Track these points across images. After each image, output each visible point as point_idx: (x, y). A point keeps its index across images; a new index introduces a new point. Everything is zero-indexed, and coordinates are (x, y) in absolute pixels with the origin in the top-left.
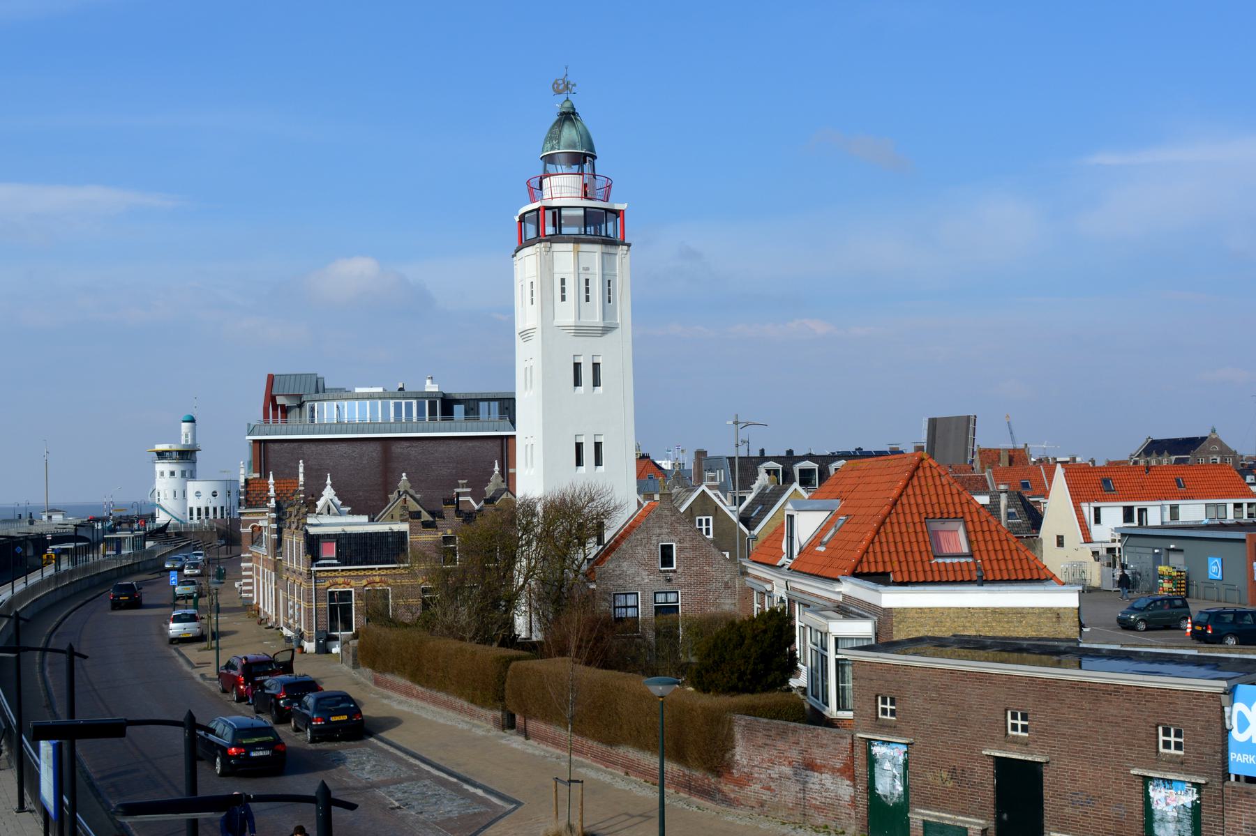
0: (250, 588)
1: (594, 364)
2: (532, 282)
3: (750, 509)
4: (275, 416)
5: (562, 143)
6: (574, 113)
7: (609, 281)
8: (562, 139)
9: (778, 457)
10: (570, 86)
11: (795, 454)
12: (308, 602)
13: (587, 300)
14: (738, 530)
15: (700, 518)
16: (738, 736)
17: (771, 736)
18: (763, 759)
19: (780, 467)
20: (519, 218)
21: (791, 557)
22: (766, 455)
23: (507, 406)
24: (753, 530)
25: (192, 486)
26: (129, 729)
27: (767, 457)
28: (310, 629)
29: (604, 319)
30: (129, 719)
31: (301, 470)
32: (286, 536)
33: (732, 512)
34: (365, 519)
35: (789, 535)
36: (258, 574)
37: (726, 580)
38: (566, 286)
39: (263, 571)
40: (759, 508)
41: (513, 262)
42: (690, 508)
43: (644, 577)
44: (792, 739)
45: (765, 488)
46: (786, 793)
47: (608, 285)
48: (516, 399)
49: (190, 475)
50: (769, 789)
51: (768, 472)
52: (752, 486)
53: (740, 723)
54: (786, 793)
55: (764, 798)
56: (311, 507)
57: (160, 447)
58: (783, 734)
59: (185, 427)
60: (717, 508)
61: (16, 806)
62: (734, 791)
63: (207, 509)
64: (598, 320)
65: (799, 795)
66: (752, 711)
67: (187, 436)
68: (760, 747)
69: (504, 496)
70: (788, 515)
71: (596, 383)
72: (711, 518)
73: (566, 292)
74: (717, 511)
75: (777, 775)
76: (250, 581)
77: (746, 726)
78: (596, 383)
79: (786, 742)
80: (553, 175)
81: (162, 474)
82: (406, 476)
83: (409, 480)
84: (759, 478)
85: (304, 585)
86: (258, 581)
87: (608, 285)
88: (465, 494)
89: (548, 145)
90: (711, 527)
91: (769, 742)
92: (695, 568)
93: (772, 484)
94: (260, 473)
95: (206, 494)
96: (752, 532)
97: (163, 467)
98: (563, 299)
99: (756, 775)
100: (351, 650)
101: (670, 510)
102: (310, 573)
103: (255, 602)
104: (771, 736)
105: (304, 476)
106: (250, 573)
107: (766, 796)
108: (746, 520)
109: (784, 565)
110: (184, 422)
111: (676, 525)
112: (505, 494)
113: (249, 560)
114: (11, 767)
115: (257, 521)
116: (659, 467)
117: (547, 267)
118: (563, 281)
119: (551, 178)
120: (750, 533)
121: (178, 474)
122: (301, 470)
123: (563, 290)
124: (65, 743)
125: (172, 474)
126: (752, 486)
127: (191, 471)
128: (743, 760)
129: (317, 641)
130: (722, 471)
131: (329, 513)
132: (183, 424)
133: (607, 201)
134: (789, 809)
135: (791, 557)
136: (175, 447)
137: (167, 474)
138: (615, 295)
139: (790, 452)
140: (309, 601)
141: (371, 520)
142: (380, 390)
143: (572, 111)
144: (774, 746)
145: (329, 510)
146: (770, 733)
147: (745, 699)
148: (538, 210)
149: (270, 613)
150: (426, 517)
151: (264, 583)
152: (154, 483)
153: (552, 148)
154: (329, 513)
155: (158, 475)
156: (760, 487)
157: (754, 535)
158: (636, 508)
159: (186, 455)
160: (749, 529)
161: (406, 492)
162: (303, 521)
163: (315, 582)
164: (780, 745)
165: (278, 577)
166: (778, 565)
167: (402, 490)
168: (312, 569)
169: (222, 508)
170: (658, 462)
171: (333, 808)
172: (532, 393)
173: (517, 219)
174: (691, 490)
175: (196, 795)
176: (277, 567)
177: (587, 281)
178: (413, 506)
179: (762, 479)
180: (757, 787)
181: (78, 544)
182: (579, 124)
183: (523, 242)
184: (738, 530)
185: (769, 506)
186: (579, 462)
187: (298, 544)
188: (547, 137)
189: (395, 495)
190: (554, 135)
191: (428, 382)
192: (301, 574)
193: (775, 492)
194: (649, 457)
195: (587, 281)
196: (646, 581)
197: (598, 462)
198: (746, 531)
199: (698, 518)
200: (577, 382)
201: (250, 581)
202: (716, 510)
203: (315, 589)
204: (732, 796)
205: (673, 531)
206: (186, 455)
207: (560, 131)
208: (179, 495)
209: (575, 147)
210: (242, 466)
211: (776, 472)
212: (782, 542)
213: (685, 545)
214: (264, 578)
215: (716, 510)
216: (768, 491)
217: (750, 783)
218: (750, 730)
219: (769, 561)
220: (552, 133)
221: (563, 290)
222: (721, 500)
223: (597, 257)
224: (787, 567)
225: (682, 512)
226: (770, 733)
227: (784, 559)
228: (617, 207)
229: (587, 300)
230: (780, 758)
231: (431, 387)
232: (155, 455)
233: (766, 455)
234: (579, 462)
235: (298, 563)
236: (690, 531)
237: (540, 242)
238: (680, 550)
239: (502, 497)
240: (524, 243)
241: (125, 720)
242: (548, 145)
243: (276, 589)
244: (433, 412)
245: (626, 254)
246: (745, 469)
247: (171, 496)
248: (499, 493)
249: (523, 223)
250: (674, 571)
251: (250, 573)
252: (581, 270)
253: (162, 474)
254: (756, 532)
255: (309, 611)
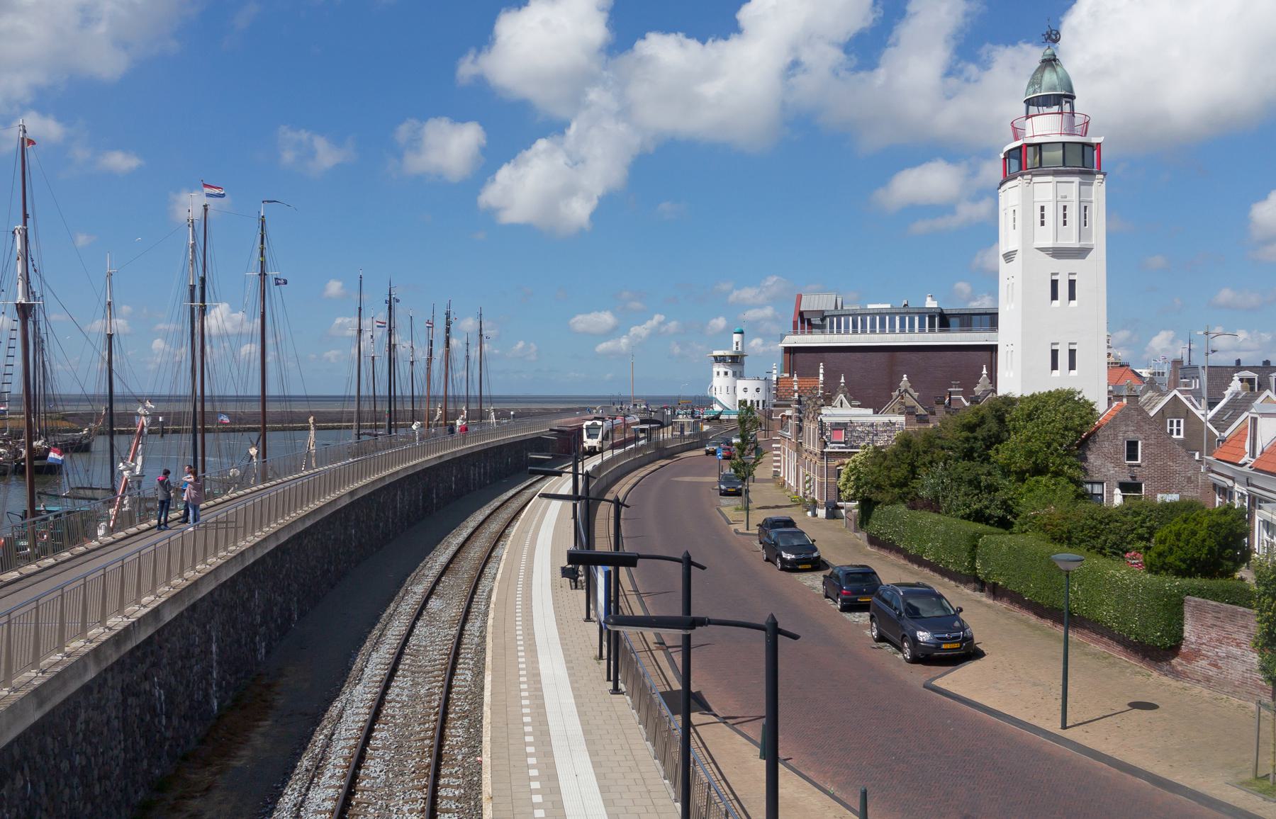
0: (779, 464)
1: (1070, 281)
2: (1014, 211)
3: (1222, 413)
4: (803, 328)
5: (1043, 87)
6: (1055, 60)
7: (1085, 207)
8: (1044, 83)
9: (1254, 367)
10: (1046, 36)
11: (1272, 365)
12: (821, 477)
13: (1065, 223)
14: (1205, 429)
15: (1178, 437)
16: (1187, 615)
17: (1220, 618)
18: (1211, 639)
19: (1256, 376)
20: (1004, 154)
21: (1254, 456)
22: (1242, 365)
23: (991, 320)
24: (1224, 432)
25: (741, 384)
26: (640, 562)
27: (1243, 367)
28: (822, 499)
29: (1080, 241)
30: (640, 554)
31: (821, 371)
32: (806, 423)
33: (1203, 413)
34: (870, 411)
35: (1252, 436)
36: (784, 453)
37: (1189, 475)
38: (1045, 213)
39: (788, 450)
40: (1231, 412)
41: (998, 194)
42: (1162, 410)
43: (1110, 469)
44: (1241, 623)
45: (1237, 394)
46: (1233, 672)
47: (1084, 210)
48: (999, 315)
49: (739, 375)
50: (1216, 666)
51: (1241, 380)
52: (1225, 392)
53: (1192, 600)
54: (1233, 672)
55: (1211, 673)
56: (828, 401)
57: (717, 353)
58: (1232, 617)
59: (736, 337)
60: (1188, 410)
61: (585, 617)
62: (1181, 664)
63: (758, 402)
64: (1074, 242)
65: (1246, 674)
66: (1201, 593)
67: (737, 344)
68: (1209, 627)
69: (990, 396)
70: (1252, 418)
71: (1072, 296)
72: (1182, 421)
73: (1045, 217)
74: (1188, 414)
75: (1224, 655)
76: (779, 458)
77: (1195, 607)
78: (1072, 296)
79: (1234, 625)
80: (1034, 116)
81: (718, 373)
82: (907, 377)
83: (909, 380)
84: (1232, 384)
85: (819, 463)
86: (784, 458)
87: (1084, 210)
88: (957, 393)
89: (1031, 90)
90: (1169, 428)
91: (1219, 623)
92: (1159, 463)
93: (1244, 391)
94: (790, 373)
95: (752, 390)
96: (1222, 434)
97: (719, 368)
98: (1043, 224)
99: (1204, 652)
100: (853, 518)
101: (1136, 410)
102: (823, 453)
103: (782, 475)
104: (1220, 618)
105: (824, 376)
106: (778, 452)
107: (1212, 672)
108: (1218, 422)
109: (1246, 464)
110: (735, 333)
111: (1142, 424)
112: (991, 394)
113: (778, 442)
114: (583, 589)
115: (784, 411)
116: (1138, 375)
117: (1028, 198)
118: (1042, 208)
119: (1033, 118)
120: (1220, 435)
121: (730, 372)
122: (821, 371)
123: (1042, 216)
124: (611, 568)
125: (726, 373)
126: (1225, 392)
127: (740, 372)
128: (1191, 637)
129: (827, 509)
130: (1198, 381)
131: (841, 406)
132: (735, 335)
133: (1085, 136)
134: (1235, 686)
135: (1254, 456)
136: (728, 353)
137: (722, 374)
138: (1091, 220)
139: (1267, 363)
140: (822, 476)
141: (876, 412)
142: (888, 306)
143: (1053, 57)
144: (1223, 628)
145: (841, 403)
146: (1219, 615)
147: (1198, 582)
148: (1020, 148)
149: (792, 484)
150: (921, 411)
151: (788, 460)
152: (712, 380)
153: (1034, 93)
154: (841, 406)
155: (715, 374)
156: (1232, 394)
157: (1224, 437)
158: (1107, 407)
159: (736, 361)
160: (1220, 432)
161: (906, 391)
162: (819, 411)
163: (827, 461)
164: (1229, 627)
165: (799, 456)
166: (1240, 463)
167: (902, 389)
168: (825, 450)
169: (764, 401)
170: (1138, 371)
171: (779, 636)
172: (1012, 306)
173: (1002, 156)
174: (1163, 395)
175: (690, 615)
176: (799, 447)
177: (1065, 207)
178: (909, 401)
179: (1236, 385)
180: (1204, 663)
181: (652, 426)
182: (1059, 69)
183: (1008, 175)
184: (1205, 429)
185: (1240, 411)
186: (1054, 366)
187: (814, 429)
188: (1029, 83)
189: (897, 393)
190: (1035, 81)
191: (929, 299)
192: (816, 455)
193: (1247, 398)
194: (1128, 366)
195: (1065, 207)
196: (1112, 472)
197: (1072, 366)
198: (1217, 433)
199: (1168, 421)
200: (1054, 296)
201: (779, 458)
202: (1187, 413)
203: (827, 466)
204: (1179, 668)
205: (1139, 428)
206: (736, 361)
207: (1042, 77)
208: (731, 390)
209: (1055, 89)
210: (775, 367)
211: (1250, 381)
212: (1245, 442)
213: (1150, 441)
214: (788, 457)
215: (1187, 413)
216: (1240, 397)
217: (1198, 659)
218: (1199, 611)
219: (1232, 459)
220: (1034, 79)
221: (1042, 216)
222: (1193, 405)
223: (1075, 187)
224: (1249, 465)
225: (1152, 415)
226: (1219, 615)
227: (1246, 458)
228: (1095, 140)
229: (1065, 223)
230: (1228, 638)
231: (931, 304)
232: (713, 359)
233: (1242, 365)
234: (1054, 366)
235: (814, 446)
236: (1155, 429)
237: (1022, 175)
238: (1144, 446)
239: (988, 396)
240: (1007, 177)
241: (637, 554)
242: (1031, 90)
243: (797, 466)
244: (932, 325)
245: (1102, 183)
246: (1220, 376)
247: (724, 390)
248: (986, 392)
249: (1007, 160)
250: (1139, 466)
251: (778, 452)
252: (1059, 198)
253: (718, 373)
254: (1226, 434)
255: (821, 484)
